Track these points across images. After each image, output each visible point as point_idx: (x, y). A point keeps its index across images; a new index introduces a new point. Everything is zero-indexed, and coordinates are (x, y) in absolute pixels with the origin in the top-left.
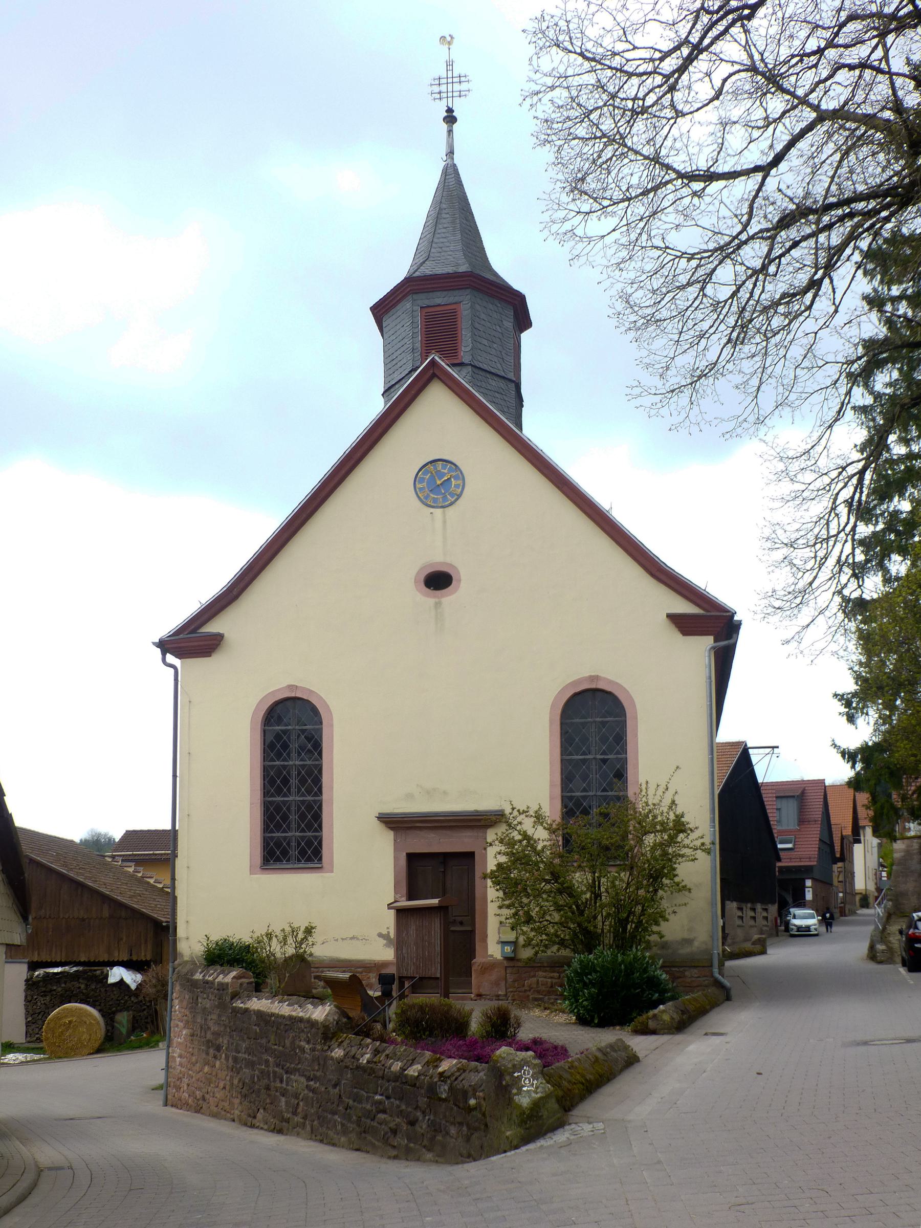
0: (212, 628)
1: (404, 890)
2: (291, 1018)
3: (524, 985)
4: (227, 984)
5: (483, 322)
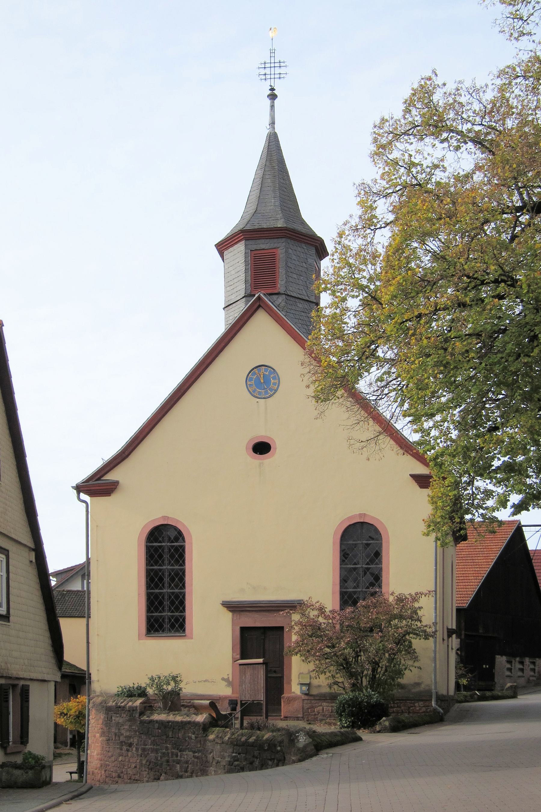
0: (111, 477)
1: (238, 651)
2: (182, 722)
3: (314, 711)
4: (137, 707)
5: (294, 262)
